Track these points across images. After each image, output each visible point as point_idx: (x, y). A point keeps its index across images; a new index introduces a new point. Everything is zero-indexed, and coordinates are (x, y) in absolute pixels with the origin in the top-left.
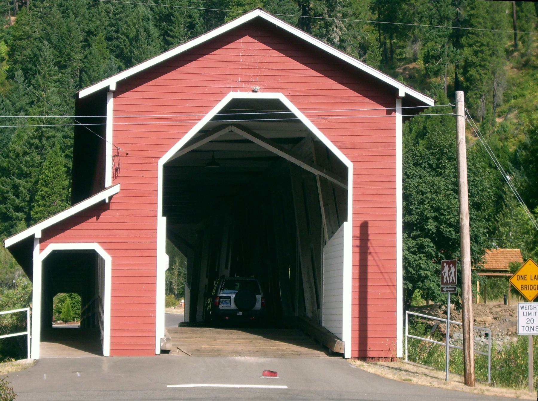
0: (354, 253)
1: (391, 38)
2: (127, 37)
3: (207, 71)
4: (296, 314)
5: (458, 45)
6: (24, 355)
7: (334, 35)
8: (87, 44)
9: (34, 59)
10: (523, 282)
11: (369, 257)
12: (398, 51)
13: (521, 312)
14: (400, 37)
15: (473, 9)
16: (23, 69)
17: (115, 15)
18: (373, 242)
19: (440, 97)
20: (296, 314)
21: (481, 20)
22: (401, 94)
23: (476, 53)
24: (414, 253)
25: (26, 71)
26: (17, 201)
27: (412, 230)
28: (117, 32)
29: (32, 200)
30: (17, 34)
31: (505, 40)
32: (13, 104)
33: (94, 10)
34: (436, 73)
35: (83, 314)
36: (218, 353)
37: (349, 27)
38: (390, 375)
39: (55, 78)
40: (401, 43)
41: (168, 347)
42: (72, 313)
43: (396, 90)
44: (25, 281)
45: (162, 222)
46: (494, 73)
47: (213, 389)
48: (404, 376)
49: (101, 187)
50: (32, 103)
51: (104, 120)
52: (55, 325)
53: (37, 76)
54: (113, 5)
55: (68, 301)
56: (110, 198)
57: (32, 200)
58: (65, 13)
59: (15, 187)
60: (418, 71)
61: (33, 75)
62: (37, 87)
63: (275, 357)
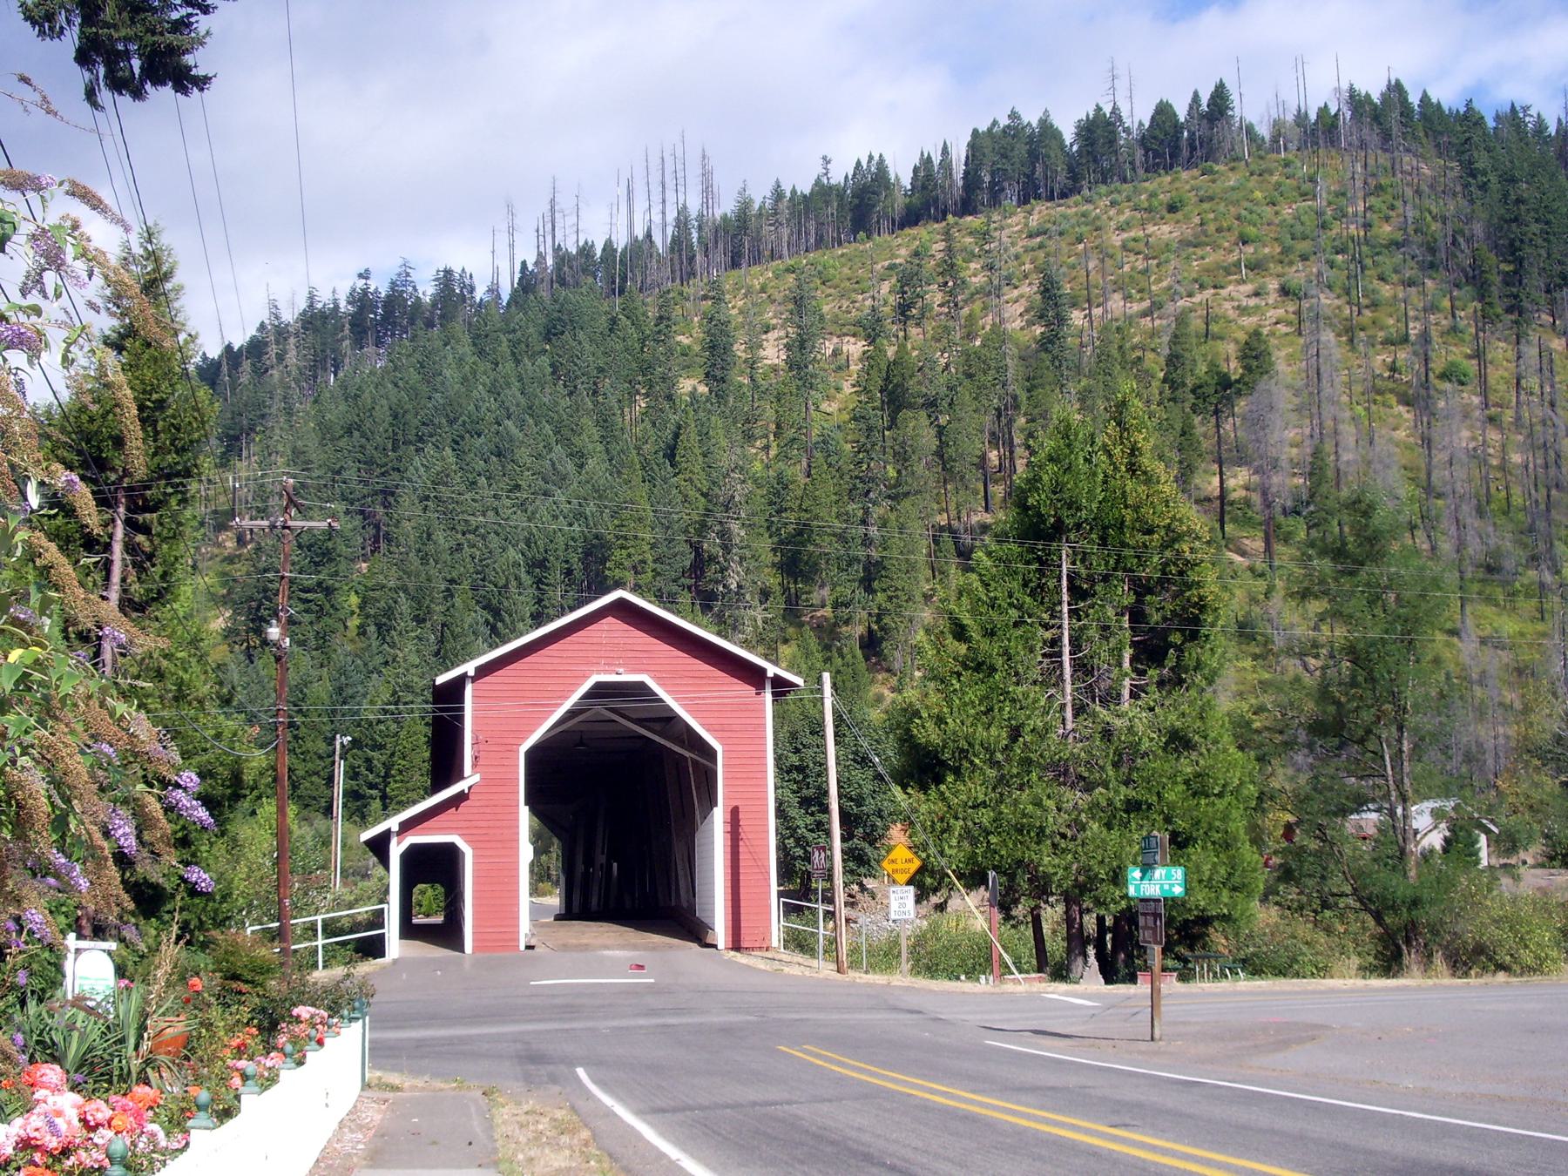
0: (725, 839)
1: (796, 583)
2: (496, 586)
3: (569, 654)
4: (673, 904)
5: (869, 590)
6: (382, 954)
7: (730, 581)
8: (449, 594)
9: (389, 613)
10: (894, 866)
11: (741, 843)
12: (804, 597)
13: (892, 896)
14: (805, 582)
15: (885, 549)
16: (376, 624)
17: (481, 561)
18: (746, 829)
19: (1132, 454)
20: (673, 904)
21: (894, 562)
22: (770, 674)
23: (890, 598)
24: (812, 831)
25: (379, 626)
26: (371, 776)
27: (810, 805)
28: (483, 580)
29: (387, 775)
30: (369, 585)
31: (923, 583)
32: (366, 665)
33: (457, 556)
34: (847, 622)
35: (446, 908)
36: (585, 948)
37: (748, 571)
38: (762, 965)
39: (413, 634)
40: (807, 588)
41: (533, 943)
42: (434, 906)
43: (763, 671)
44: (380, 870)
45: (524, 812)
46: (911, 621)
47: (578, 984)
48: (776, 965)
49: (461, 777)
50: (386, 663)
51: (462, 709)
52: (415, 921)
53: (393, 632)
54: (478, 549)
55: (430, 892)
56: (470, 788)
57: (387, 775)
58: (424, 560)
59: (368, 760)
60: (826, 619)
61: (388, 631)
62: (393, 645)
63: (645, 950)
